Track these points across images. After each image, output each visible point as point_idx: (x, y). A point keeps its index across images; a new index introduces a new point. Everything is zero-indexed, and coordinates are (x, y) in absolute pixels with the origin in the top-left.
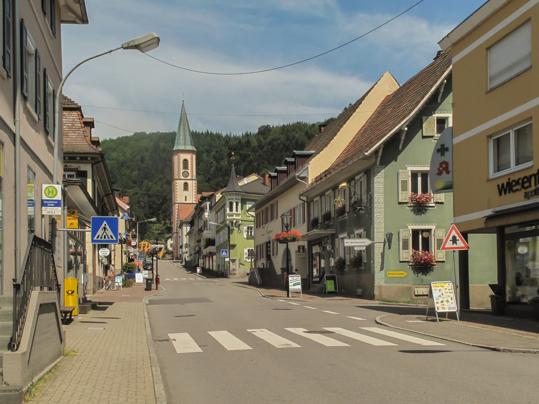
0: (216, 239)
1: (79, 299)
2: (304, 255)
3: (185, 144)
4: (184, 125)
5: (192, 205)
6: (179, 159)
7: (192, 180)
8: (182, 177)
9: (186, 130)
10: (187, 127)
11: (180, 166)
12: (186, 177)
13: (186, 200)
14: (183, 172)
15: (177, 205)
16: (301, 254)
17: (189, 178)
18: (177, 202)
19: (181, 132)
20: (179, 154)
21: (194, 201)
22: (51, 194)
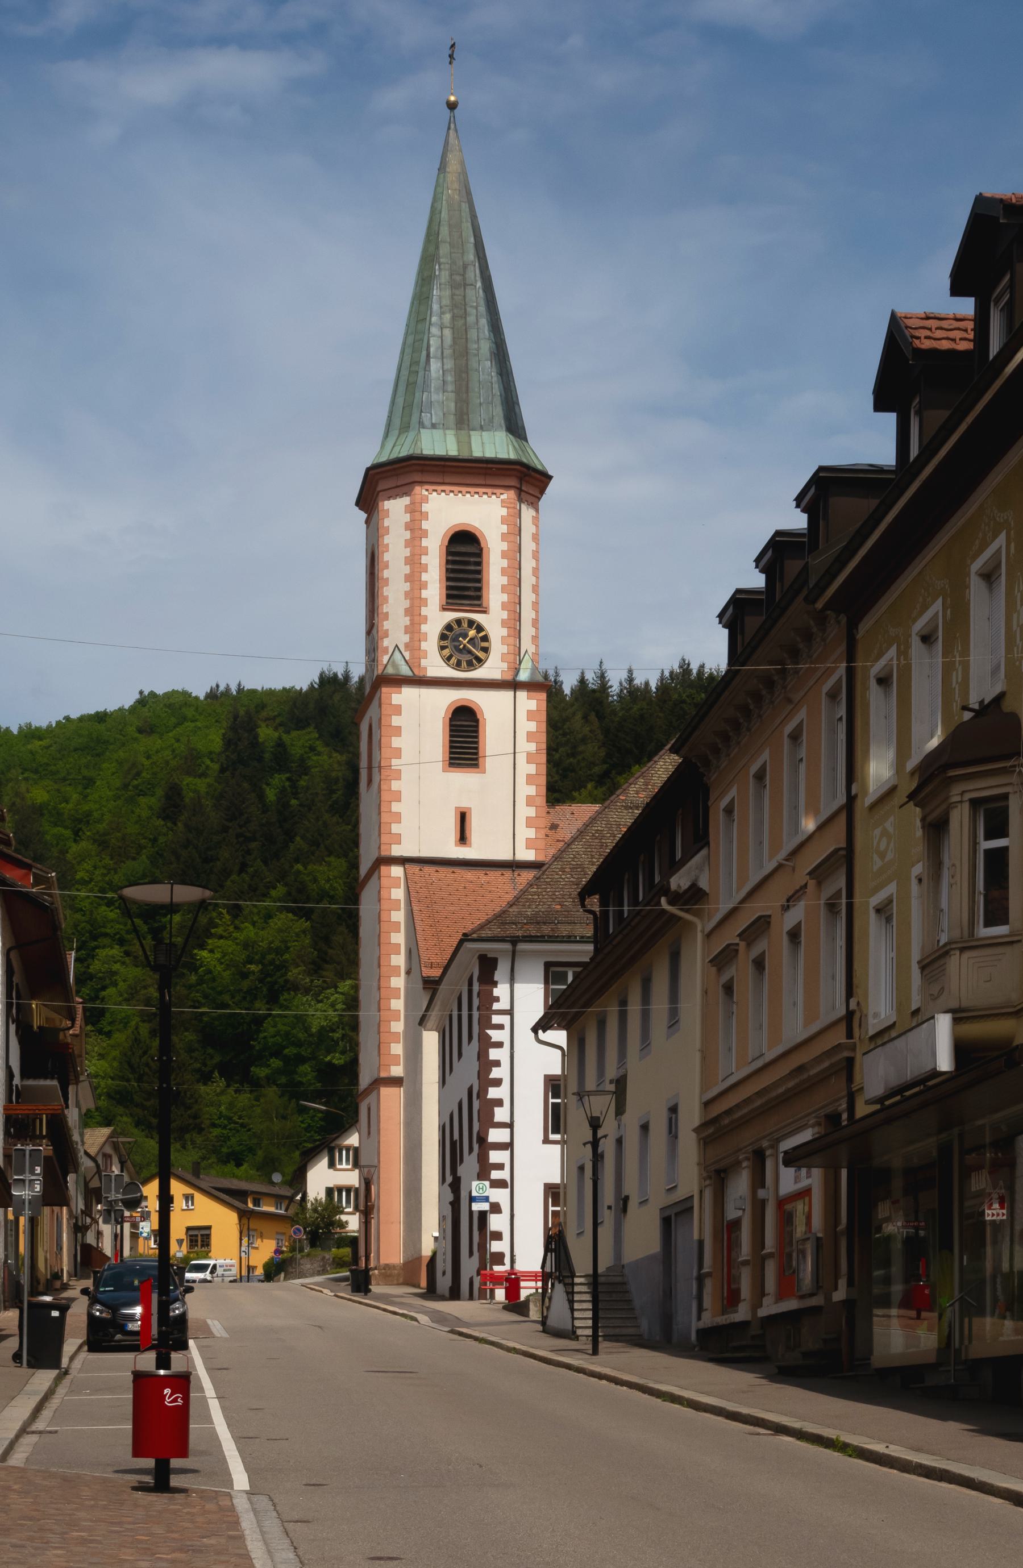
0: (822, 1112)
1: (16, 1367)
2: (1003, 1215)
3: (462, 421)
4: (458, 284)
5: (508, 873)
6: (416, 531)
7: (513, 685)
8: (436, 666)
9: (471, 319)
10: (476, 294)
11: (424, 585)
12: (471, 666)
13: (463, 838)
14: (449, 627)
15: (397, 871)
16: (994, 1212)
17: (493, 668)
18: (396, 851)
19: (434, 330)
20: (421, 491)
21: (521, 844)
22: (481, 1190)
